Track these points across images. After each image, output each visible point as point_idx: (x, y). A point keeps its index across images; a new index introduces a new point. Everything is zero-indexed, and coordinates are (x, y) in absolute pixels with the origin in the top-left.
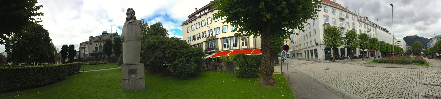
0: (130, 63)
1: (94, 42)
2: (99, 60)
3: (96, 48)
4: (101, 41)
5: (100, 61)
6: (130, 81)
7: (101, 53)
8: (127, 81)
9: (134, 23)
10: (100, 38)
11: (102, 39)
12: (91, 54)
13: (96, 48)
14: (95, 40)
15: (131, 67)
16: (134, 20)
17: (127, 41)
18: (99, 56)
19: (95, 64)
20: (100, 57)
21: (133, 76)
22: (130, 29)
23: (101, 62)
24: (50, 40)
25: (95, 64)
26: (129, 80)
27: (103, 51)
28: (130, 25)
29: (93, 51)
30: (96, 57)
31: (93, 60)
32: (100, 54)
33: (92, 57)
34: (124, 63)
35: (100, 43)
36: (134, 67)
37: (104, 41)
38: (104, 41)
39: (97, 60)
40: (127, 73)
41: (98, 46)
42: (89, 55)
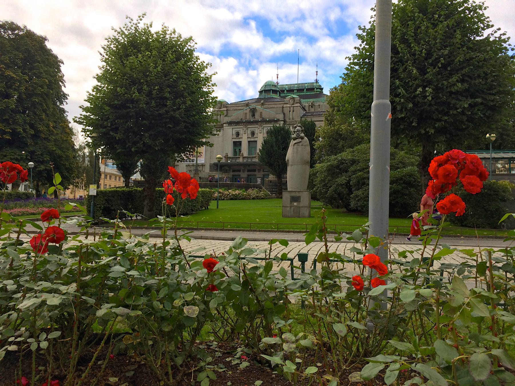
0: (294, 190)
1: (230, 123)
2: (247, 188)
3: (237, 144)
4: (256, 122)
5: (250, 191)
6: (292, 208)
7: (254, 164)
8: (289, 209)
9: (301, 144)
10: (253, 111)
11: (257, 117)
12: (218, 166)
13: (237, 144)
14: (235, 116)
15: (293, 194)
16: (300, 140)
17: (292, 165)
18: (244, 175)
19: (235, 198)
20: (249, 179)
21: (295, 204)
22: (295, 150)
23: (252, 192)
24: (61, 79)
25: (235, 198)
26: (291, 207)
27: (261, 158)
28: (295, 146)
29: (227, 157)
30: (234, 179)
31: (228, 187)
32: (249, 167)
33: (217, 175)
34: (288, 190)
35: (252, 128)
36: (297, 194)
37: (264, 121)
38: (264, 121)
39: (239, 187)
40: (289, 200)
41: (244, 141)
42: (207, 169)
